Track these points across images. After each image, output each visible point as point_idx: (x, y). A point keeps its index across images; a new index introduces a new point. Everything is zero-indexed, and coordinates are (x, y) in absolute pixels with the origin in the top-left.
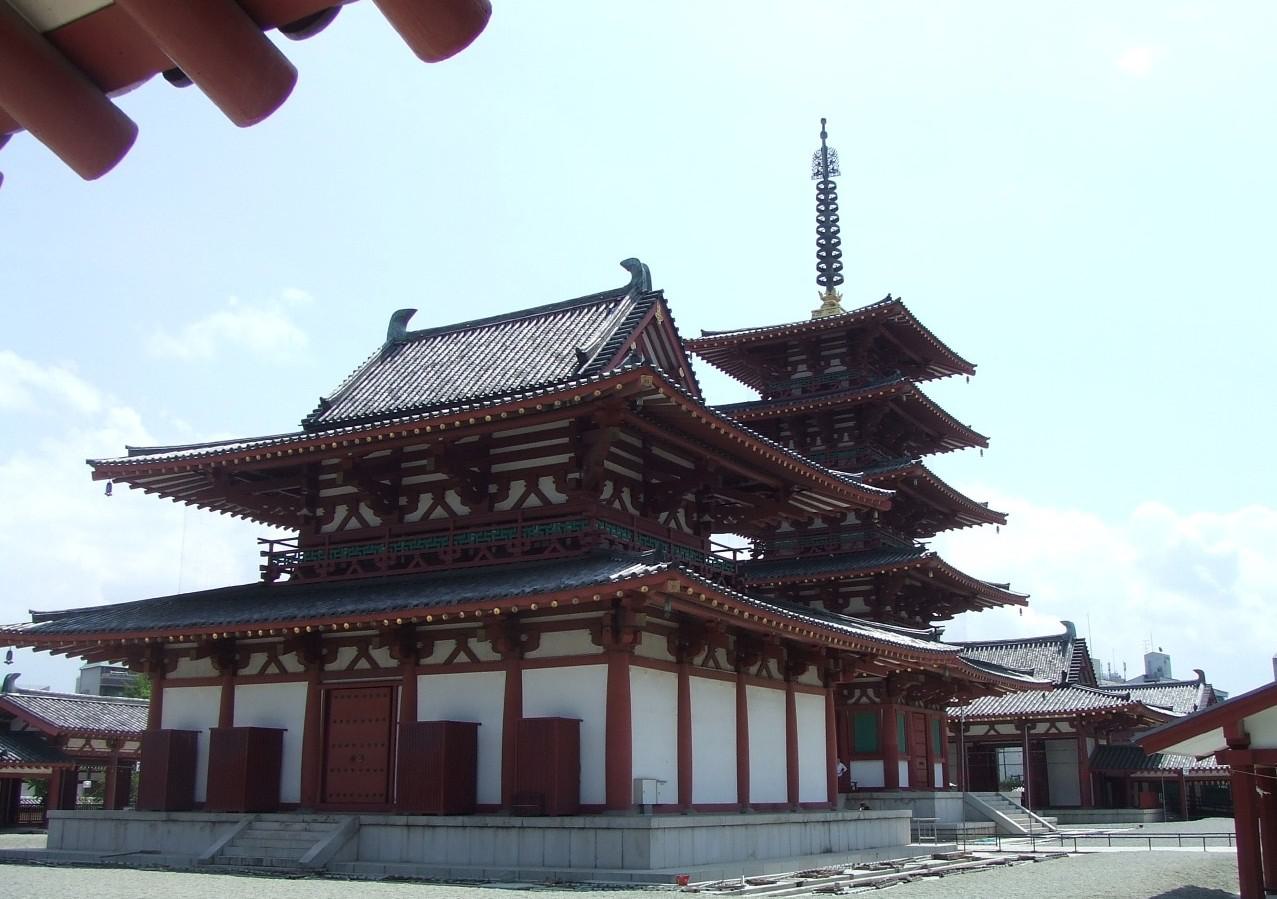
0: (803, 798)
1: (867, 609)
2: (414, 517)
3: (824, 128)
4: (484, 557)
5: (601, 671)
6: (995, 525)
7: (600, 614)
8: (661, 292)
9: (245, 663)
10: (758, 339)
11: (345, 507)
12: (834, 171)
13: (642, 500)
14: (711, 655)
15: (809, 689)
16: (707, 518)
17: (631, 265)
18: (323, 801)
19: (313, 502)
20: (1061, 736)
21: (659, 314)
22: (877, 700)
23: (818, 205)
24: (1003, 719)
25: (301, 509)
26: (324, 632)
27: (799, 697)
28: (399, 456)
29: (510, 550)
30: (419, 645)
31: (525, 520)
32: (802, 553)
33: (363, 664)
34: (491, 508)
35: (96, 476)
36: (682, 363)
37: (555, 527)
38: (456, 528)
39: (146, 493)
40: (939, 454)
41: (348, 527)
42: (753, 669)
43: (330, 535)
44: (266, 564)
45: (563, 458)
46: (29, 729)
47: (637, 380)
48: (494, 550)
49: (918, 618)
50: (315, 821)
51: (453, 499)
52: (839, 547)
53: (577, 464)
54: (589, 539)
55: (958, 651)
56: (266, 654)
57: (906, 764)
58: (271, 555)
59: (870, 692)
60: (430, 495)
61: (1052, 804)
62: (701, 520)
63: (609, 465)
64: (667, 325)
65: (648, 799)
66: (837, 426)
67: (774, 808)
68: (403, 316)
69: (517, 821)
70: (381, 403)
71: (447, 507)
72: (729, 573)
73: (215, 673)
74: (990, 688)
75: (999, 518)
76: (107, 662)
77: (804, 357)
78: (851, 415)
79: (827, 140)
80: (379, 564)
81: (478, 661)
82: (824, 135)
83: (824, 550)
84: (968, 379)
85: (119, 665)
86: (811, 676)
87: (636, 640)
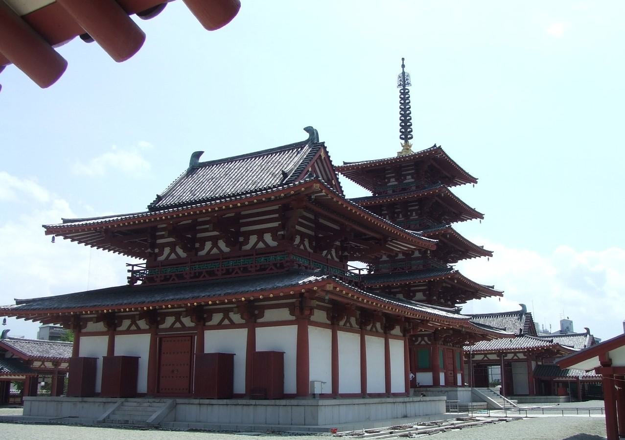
0: (393, 391)
1: (425, 298)
2: (203, 253)
3: (403, 62)
4: (237, 273)
5: (294, 329)
6: (487, 257)
7: (294, 300)
8: (324, 143)
9: (120, 325)
10: (371, 166)
11: (169, 248)
12: (408, 84)
13: (314, 245)
14: (348, 321)
15: (396, 337)
16: (346, 253)
17: (309, 130)
18: (158, 392)
19: (153, 246)
20: (519, 360)
21: (322, 154)
22: (429, 343)
23: (401, 100)
24: (491, 352)
25: (147, 249)
26: (159, 309)
27: (391, 341)
28: (195, 223)
29: (250, 269)
30: (205, 316)
31: (257, 255)
32: (392, 271)
33: (178, 325)
34: (240, 249)
35: (47, 233)
36: (334, 178)
37: (272, 258)
38: (223, 259)
39: (72, 241)
40: (459, 222)
41: (170, 258)
42: (369, 328)
43: (162, 262)
44: (130, 276)
45: (276, 224)
46: (14, 357)
47: (312, 186)
48: (242, 269)
49: (449, 303)
50: (154, 402)
51: (222, 244)
52: (411, 268)
53: (283, 227)
54: (288, 264)
55: (469, 319)
56: (130, 320)
57: (444, 374)
58: (133, 271)
59: (426, 339)
60: (210, 242)
61: (515, 393)
62: (343, 255)
63: (298, 228)
64: (327, 159)
65: (317, 391)
66: (410, 208)
67: (379, 395)
68: (197, 155)
69: (253, 402)
70: (187, 197)
71: (219, 248)
72: (357, 281)
73: (105, 329)
74: (485, 337)
75: (489, 254)
76: (52, 324)
77: (393, 175)
78: (417, 203)
79: (405, 69)
80: (185, 276)
81: (234, 324)
82: (403, 66)
83: (403, 269)
84: (474, 186)
85: (58, 325)
86: (397, 331)
87: (311, 313)
